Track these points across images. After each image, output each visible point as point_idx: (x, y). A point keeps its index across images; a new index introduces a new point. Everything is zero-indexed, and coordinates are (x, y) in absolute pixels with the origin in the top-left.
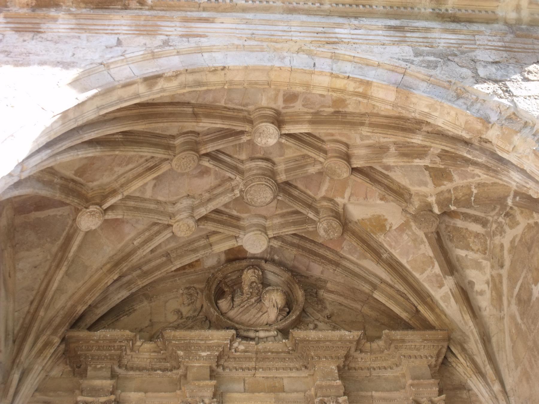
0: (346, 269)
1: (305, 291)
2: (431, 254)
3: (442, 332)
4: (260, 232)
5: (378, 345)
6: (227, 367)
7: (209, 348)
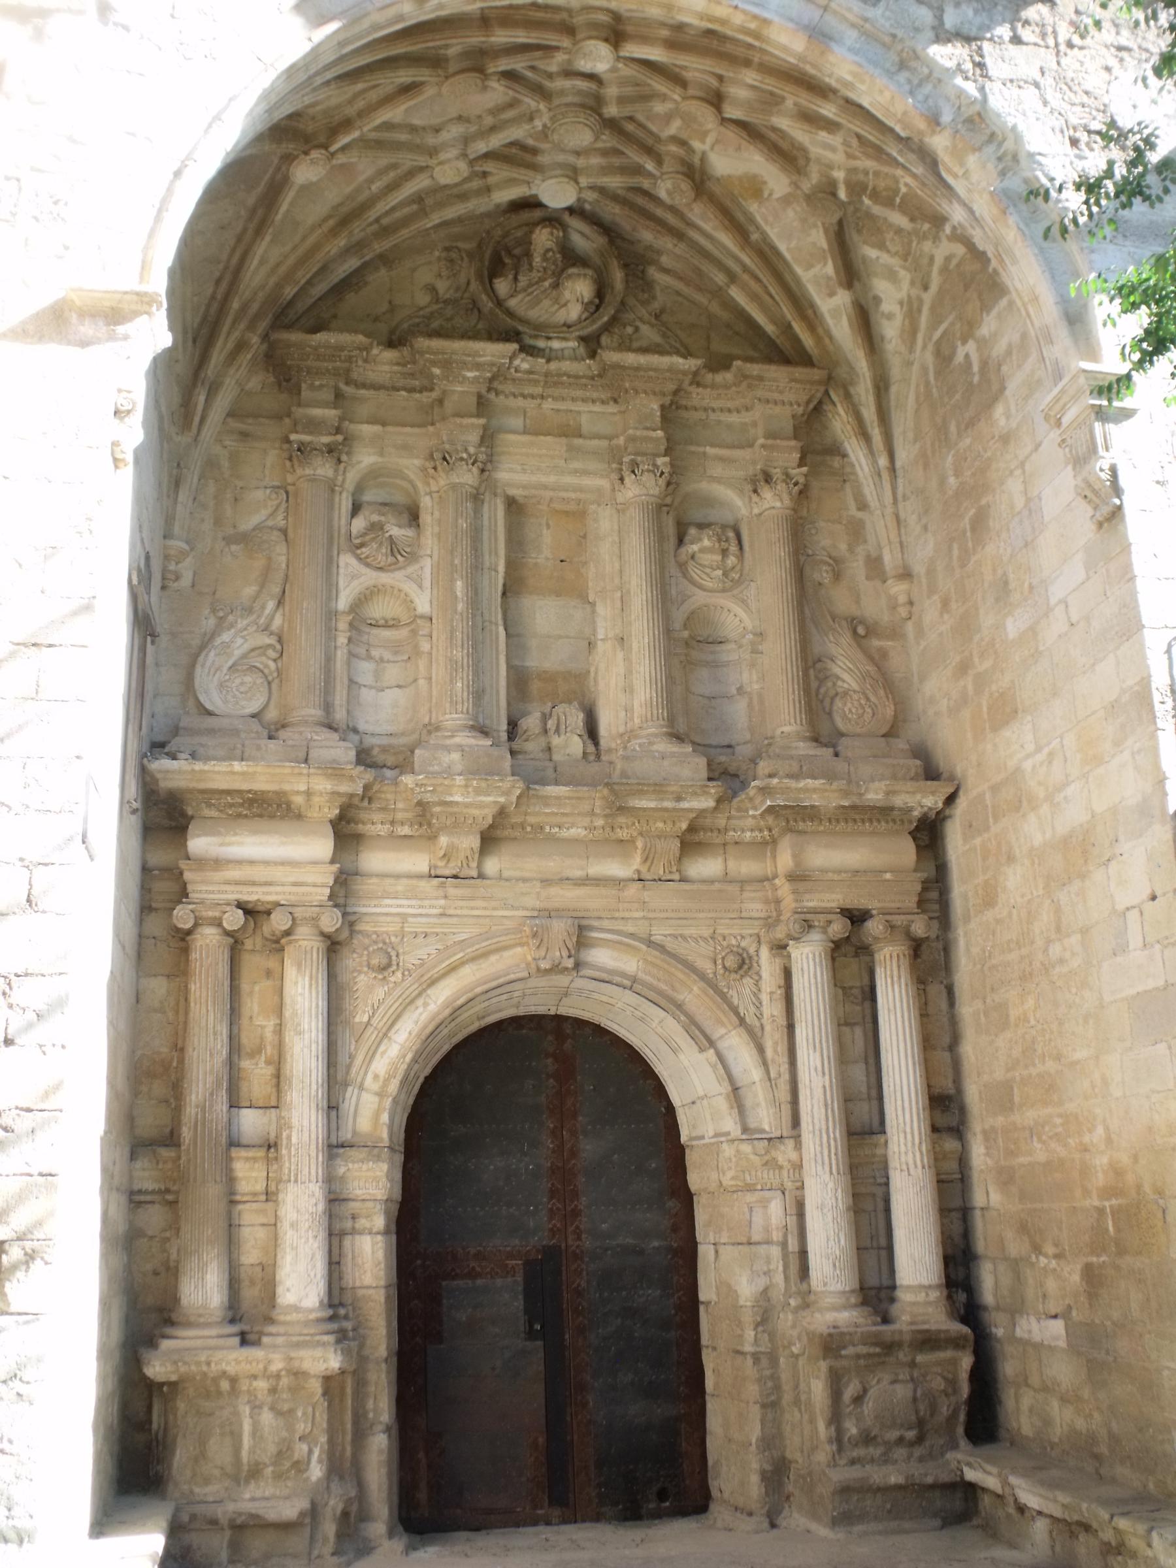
2: (825, 245)
4: (566, 180)
7: (478, 366)
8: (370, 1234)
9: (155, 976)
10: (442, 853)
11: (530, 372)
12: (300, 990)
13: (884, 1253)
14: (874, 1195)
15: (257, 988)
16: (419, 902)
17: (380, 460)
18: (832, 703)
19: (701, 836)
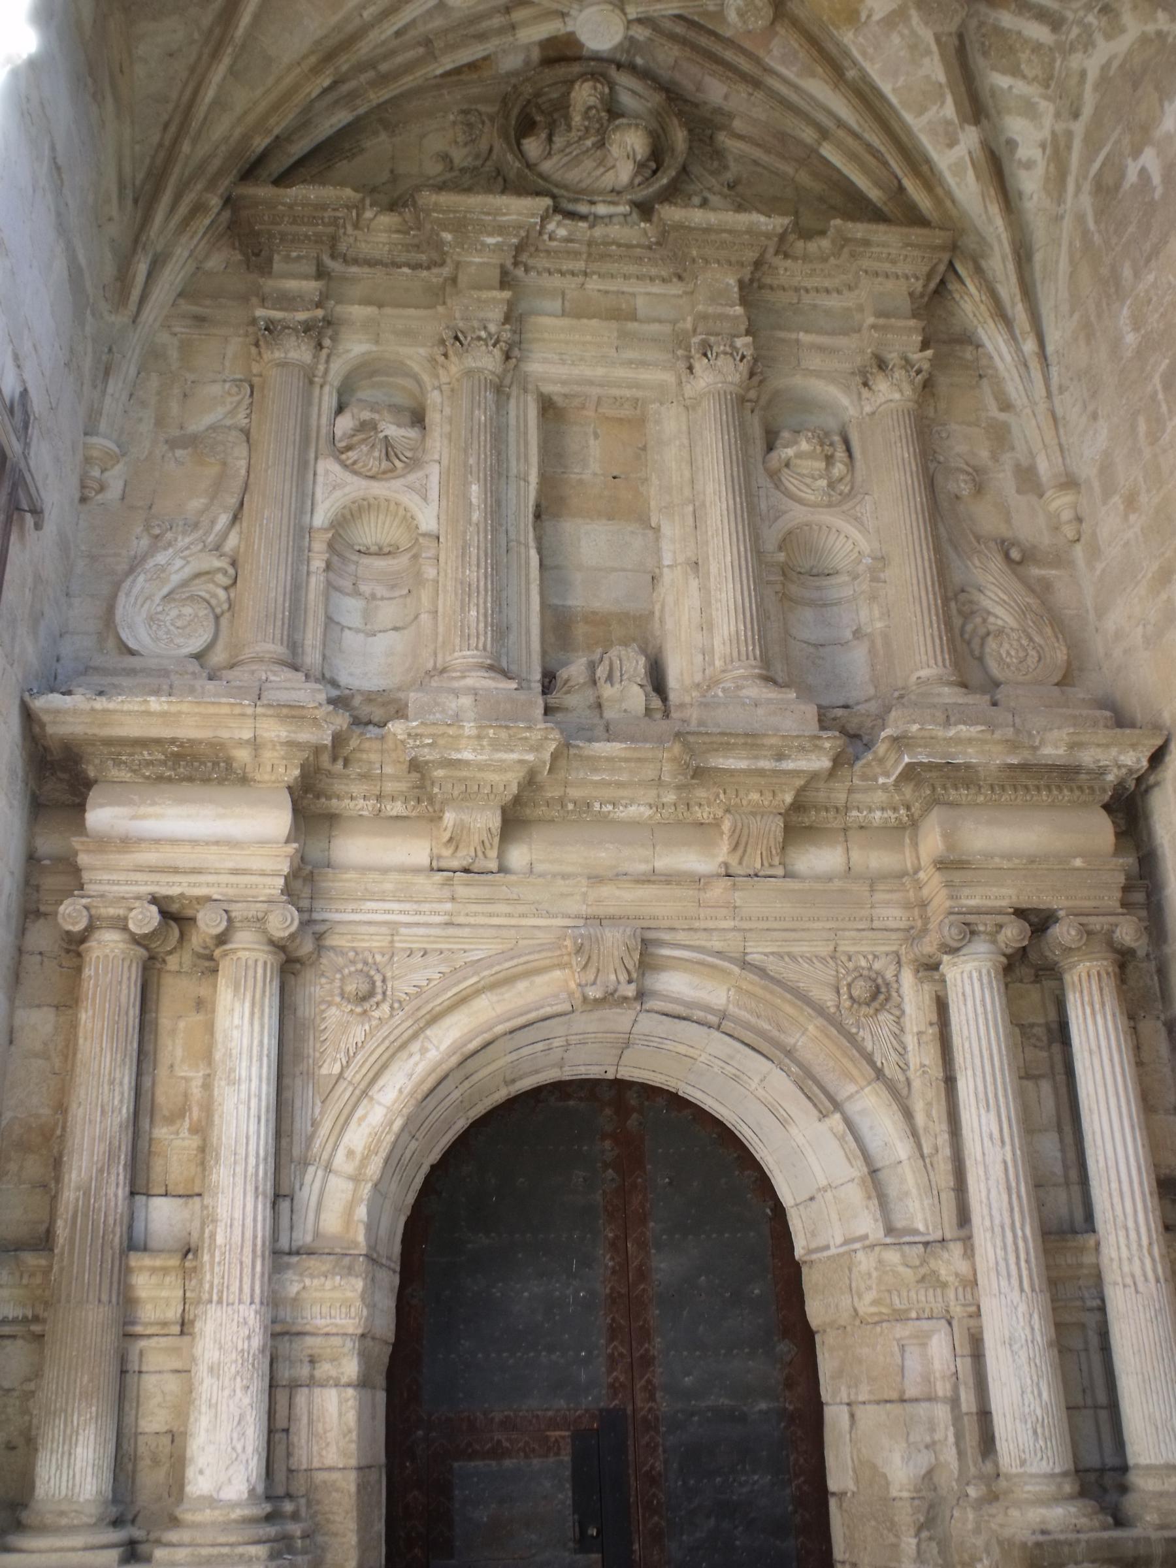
0: (772, 94)
1: (690, 131)
2: (942, 78)
3: (942, 233)
4: (611, 7)
5: (819, 247)
6: (533, 268)
7: (501, 229)
8: (336, 1386)
9: (39, 1006)
10: (447, 836)
11: (568, 240)
12: (236, 1021)
13: (1104, 1415)
14: (1083, 1326)
15: (182, 1025)
16: (415, 907)
17: (374, 348)
18: (982, 645)
19: (811, 817)
